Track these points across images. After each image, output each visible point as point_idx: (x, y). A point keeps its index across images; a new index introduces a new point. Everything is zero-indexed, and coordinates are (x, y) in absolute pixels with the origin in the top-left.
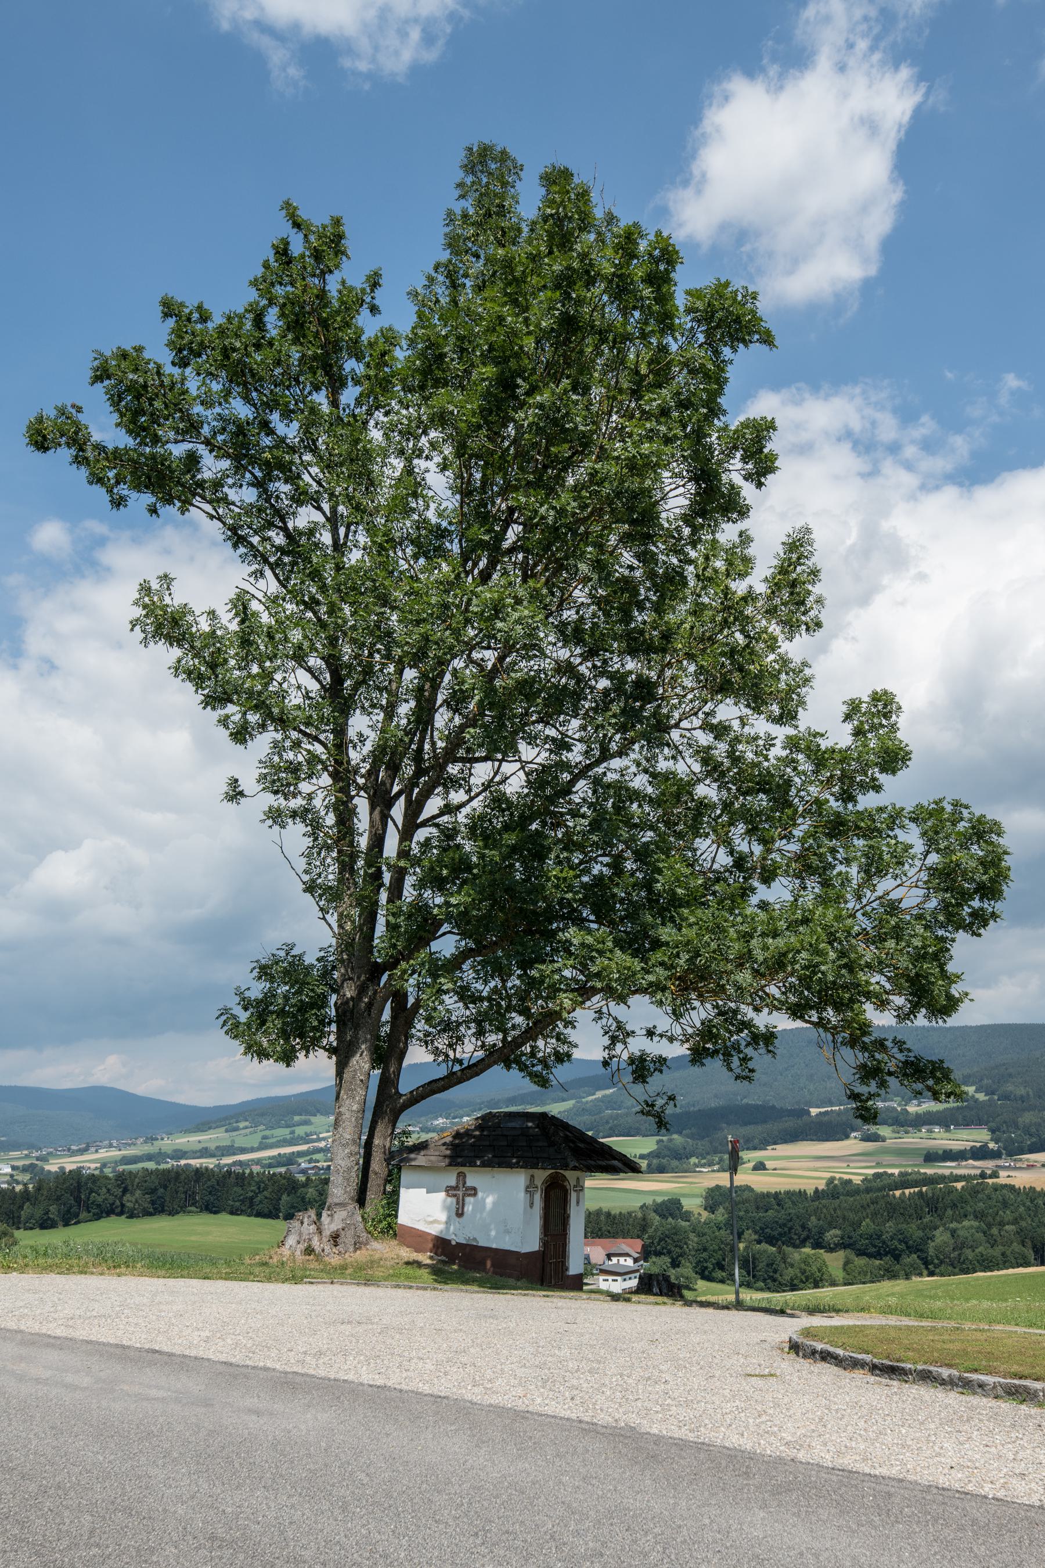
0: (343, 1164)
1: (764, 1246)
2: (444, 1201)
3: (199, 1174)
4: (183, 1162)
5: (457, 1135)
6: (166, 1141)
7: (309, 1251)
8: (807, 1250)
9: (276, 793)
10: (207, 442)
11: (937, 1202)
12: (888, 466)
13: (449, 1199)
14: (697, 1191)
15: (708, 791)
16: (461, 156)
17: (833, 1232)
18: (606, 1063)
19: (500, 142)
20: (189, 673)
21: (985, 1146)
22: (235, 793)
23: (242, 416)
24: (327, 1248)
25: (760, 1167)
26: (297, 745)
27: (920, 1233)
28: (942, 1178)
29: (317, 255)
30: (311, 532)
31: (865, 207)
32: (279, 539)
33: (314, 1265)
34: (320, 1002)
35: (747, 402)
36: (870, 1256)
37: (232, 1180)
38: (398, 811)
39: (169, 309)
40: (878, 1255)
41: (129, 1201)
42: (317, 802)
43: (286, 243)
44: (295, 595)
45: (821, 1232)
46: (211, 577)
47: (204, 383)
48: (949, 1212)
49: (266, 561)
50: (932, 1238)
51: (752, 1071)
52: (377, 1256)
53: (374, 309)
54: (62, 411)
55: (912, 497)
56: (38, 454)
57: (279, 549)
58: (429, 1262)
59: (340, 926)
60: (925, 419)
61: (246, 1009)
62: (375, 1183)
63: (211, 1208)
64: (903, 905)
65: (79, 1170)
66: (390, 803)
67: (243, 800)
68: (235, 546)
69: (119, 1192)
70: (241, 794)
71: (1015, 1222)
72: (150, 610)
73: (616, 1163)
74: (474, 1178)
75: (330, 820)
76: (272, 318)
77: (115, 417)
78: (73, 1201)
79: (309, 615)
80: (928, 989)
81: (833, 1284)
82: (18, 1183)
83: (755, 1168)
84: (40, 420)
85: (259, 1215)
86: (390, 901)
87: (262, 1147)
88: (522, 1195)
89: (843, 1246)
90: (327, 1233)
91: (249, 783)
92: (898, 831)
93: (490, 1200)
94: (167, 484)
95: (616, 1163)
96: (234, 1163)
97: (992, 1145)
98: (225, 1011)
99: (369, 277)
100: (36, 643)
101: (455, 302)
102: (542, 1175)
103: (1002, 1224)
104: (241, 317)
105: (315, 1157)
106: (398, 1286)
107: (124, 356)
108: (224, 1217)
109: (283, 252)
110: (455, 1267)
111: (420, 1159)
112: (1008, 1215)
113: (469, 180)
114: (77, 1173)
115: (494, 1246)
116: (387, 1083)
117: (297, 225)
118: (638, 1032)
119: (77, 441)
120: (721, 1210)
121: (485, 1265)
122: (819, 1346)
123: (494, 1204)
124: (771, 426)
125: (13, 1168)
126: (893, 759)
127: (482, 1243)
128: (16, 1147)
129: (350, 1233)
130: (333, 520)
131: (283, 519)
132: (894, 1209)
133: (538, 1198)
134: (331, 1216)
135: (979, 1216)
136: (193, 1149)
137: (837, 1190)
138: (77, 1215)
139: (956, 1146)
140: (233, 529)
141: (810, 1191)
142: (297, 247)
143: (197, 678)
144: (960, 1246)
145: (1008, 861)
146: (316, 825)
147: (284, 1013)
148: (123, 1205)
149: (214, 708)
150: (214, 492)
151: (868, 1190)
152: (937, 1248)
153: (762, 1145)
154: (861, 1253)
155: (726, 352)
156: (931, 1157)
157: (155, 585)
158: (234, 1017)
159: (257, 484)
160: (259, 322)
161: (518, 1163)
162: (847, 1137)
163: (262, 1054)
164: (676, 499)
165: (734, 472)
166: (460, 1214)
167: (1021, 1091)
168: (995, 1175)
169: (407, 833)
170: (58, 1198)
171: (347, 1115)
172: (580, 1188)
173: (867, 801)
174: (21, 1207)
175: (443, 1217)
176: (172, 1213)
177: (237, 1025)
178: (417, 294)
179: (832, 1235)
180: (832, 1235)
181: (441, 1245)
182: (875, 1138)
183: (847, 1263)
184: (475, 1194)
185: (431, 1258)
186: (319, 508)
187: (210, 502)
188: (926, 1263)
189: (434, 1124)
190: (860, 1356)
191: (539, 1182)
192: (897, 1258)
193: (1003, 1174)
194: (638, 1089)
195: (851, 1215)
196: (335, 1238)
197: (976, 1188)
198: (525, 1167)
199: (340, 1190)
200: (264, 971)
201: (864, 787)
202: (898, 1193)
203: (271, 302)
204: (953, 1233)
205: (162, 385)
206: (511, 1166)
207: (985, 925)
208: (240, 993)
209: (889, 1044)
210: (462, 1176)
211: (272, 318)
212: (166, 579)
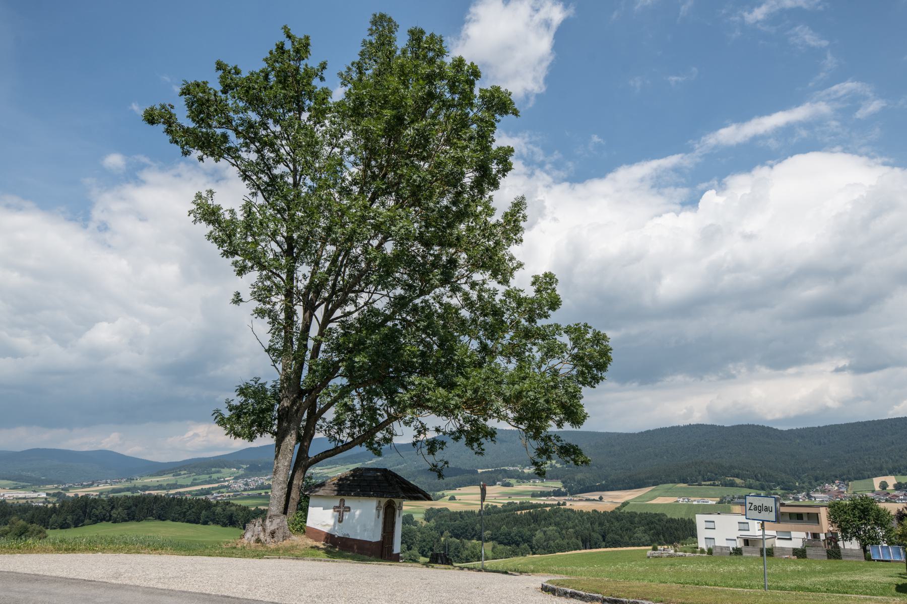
0: (277, 493)
1: (454, 539)
3: (157, 498)
4: (147, 492)
5: (341, 479)
6: (139, 481)
7: (258, 541)
8: (474, 541)
9: (260, 301)
10: (236, 130)
11: (537, 517)
12: (538, 172)
14: (421, 511)
15: (465, 313)
16: (371, 18)
17: (488, 532)
18: (414, 444)
19: (389, 14)
20: (216, 239)
21: (560, 489)
22: (238, 300)
23: (253, 119)
24: (268, 539)
25: (452, 498)
26: (269, 278)
27: (529, 533)
28: (539, 505)
29: (297, 51)
30: (282, 177)
31: (541, 61)
32: (266, 179)
33: (261, 548)
34: (270, 408)
35: (500, 140)
36: (505, 544)
37: (175, 502)
38: (320, 313)
39: (220, 66)
40: (509, 544)
41: (114, 513)
42: (277, 307)
43: (283, 44)
44: (273, 206)
46: (233, 195)
47: (235, 102)
48: (543, 522)
49: (259, 188)
50: (534, 535)
51: (483, 450)
52: (295, 544)
53: (322, 79)
54: (163, 107)
55: (548, 186)
56: (149, 126)
57: (266, 183)
58: (322, 546)
59: (283, 370)
60: (556, 152)
61: (231, 411)
62: (293, 504)
63: (161, 518)
64: (561, 372)
65: (87, 496)
66: (314, 308)
67: (241, 304)
68: (244, 180)
69: (109, 508)
70: (241, 300)
71: (573, 527)
72: (200, 206)
73: (420, 495)
75: (282, 316)
76: (272, 78)
77: (188, 113)
78: (83, 513)
79: (279, 216)
80: (573, 414)
82: (49, 503)
83: (450, 499)
84: (152, 109)
85: (189, 521)
86: (312, 358)
87: (193, 485)
90: (268, 531)
91: (246, 295)
92: (557, 336)
93: (358, 512)
94: (213, 146)
95: (420, 495)
96: (177, 493)
97: (563, 489)
98: (217, 411)
99: (321, 64)
100: (97, 214)
101: (360, 80)
102: (384, 501)
103: (567, 528)
104: (258, 75)
105: (221, 490)
106: (314, 560)
107: (198, 85)
108: (169, 522)
109: (281, 48)
111: (321, 492)
112: (570, 524)
113: (374, 28)
114: (85, 498)
115: (358, 538)
116: (302, 452)
117: (289, 36)
118: (431, 429)
119: (169, 122)
120: (433, 520)
122: (569, 590)
123: (360, 515)
124: (512, 150)
125: (47, 494)
126: (555, 304)
128: (51, 482)
129: (281, 531)
130: (295, 172)
131: (269, 169)
132: (518, 521)
134: (271, 522)
136: (153, 485)
138: (83, 521)
140: (244, 172)
142: (288, 46)
143: (220, 242)
145: (612, 355)
146: (274, 319)
147: (251, 412)
148: (111, 516)
149: (227, 257)
150: (233, 152)
151: (505, 511)
152: (537, 540)
153: (454, 487)
154: (500, 543)
155: (498, 117)
156: (534, 495)
157: (204, 194)
158: (221, 414)
159: (258, 151)
160: (266, 78)
162: (495, 484)
163: (237, 435)
164: (469, 178)
165: (494, 167)
166: (340, 521)
168: (564, 504)
169: (323, 326)
170: (73, 512)
171: (282, 468)
172: (400, 508)
173: (541, 323)
174: (50, 517)
175: (331, 522)
176: (139, 520)
177: (223, 419)
178: (342, 75)
179: (487, 533)
180: (487, 533)
182: (508, 485)
183: (494, 548)
186: (287, 166)
187: (233, 158)
188: (532, 548)
189: (333, 471)
190: (596, 595)
191: (382, 505)
192: (518, 545)
193: (568, 504)
194: (431, 459)
195: (496, 523)
196: (273, 534)
197: (556, 510)
198: (377, 496)
199: (275, 508)
200: (242, 391)
201: (540, 316)
202: (519, 512)
203: (273, 70)
204: (545, 532)
205: (216, 100)
206: (369, 496)
207: (598, 382)
208: (228, 402)
209: (552, 438)
210: (342, 501)
211: (272, 78)
212: (211, 192)
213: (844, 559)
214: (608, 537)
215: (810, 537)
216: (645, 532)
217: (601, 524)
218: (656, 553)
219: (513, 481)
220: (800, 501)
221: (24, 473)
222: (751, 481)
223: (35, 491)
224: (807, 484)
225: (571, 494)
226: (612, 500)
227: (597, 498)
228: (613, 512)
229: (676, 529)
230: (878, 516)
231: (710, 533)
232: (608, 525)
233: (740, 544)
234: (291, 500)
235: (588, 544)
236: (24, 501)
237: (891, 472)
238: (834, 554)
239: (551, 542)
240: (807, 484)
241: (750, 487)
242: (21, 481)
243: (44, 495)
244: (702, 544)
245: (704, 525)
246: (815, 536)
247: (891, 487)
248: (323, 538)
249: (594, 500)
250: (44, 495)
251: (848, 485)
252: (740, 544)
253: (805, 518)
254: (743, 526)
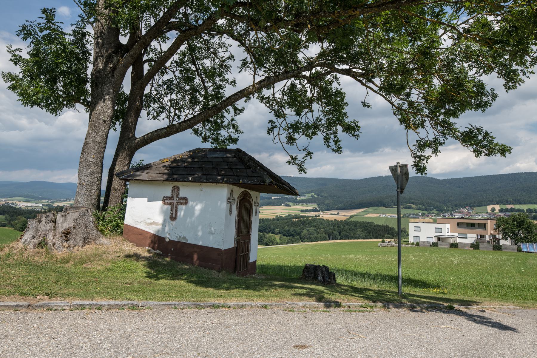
0: (86, 179)
2: (162, 208)
5: (175, 161)
8: (270, 234)
11: (304, 222)
13: (166, 207)
28: (306, 216)
36: (287, 236)
45: (274, 230)
58: (146, 254)
71: (324, 228)
74: (185, 191)
81: (277, 244)
88: (224, 205)
89: (279, 233)
93: (198, 207)
102: (238, 191)
103: (320, 229)
110: (168, 259)
111: (144, 176)
112: (322, 226)
115: (200, 244)
121: (192, 258)
123: (202, 211)
127: (190, 241)
132: (293, 224)
133: (235, 207)
135: (315, 226)
137: (278, 219)
139: (309, 208)
141: (272, 219)
144: (310, 234)
151: (286, 219)
154: (284, 235)
156: (302, 211)
161: (223, 179)
162: (281, 205)
166: (173, 217)
167: (326, 195)
168: (319, 216)
175: (160, 219)
179: (277, 230)
180: (277, 230)
181: (157, 241)
182: (288, 206)
184: (186, 203)
185: (149, 251)
188: (301, 238)
191: (236, 196)
192: (294, 236)
193: (321, 216)
196: (66, 234)
197: (315, 219)
206: (217, 182)
210: (176, 189)
213: (503, 250)
214: (342, 234)
215: (479, 237)
216: (362, 231)
217: (339, 227)
218: (384, 244)
219: (291, 204)
220: (479, 215)
221: (30, 194)
222: (420, 206)
223: (36, 203)
224: (450, 208)
225: (322, 211)
226: (343, 215)
227: (336, 213)
228: (345, 221)
229: (379, 230)
230: (528, 226)
231: (417, 234)
232: (342, 227)
233: (435, 240)
234: (113, 191)
235: (331, 237)
236: (31, 208)
237: (497, 203)
238: (497, 247)
239: (311, 236)
240: (450, 208)
241: (419, 209)
242: (28, 198)
243: (41, 205)
244: (411, 240)
245: (414, 229)
246: (483, 237)
247: (497, 211)
248: (149, 241)
249: (334, 214)
250: (41, 205)
251: (473, 209)
252: (435, 240)
253: (476, 226)
254: (439, 230)
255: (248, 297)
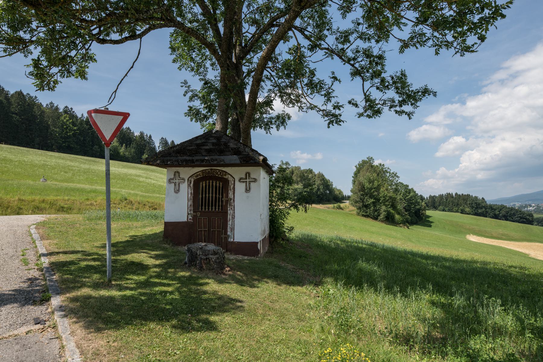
255: (191, 193)
